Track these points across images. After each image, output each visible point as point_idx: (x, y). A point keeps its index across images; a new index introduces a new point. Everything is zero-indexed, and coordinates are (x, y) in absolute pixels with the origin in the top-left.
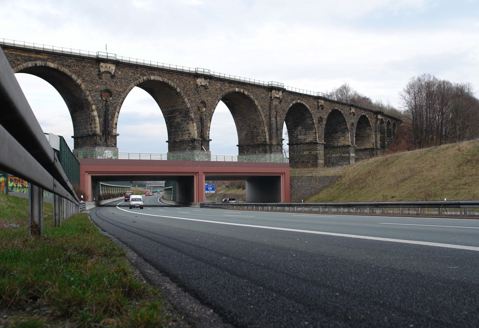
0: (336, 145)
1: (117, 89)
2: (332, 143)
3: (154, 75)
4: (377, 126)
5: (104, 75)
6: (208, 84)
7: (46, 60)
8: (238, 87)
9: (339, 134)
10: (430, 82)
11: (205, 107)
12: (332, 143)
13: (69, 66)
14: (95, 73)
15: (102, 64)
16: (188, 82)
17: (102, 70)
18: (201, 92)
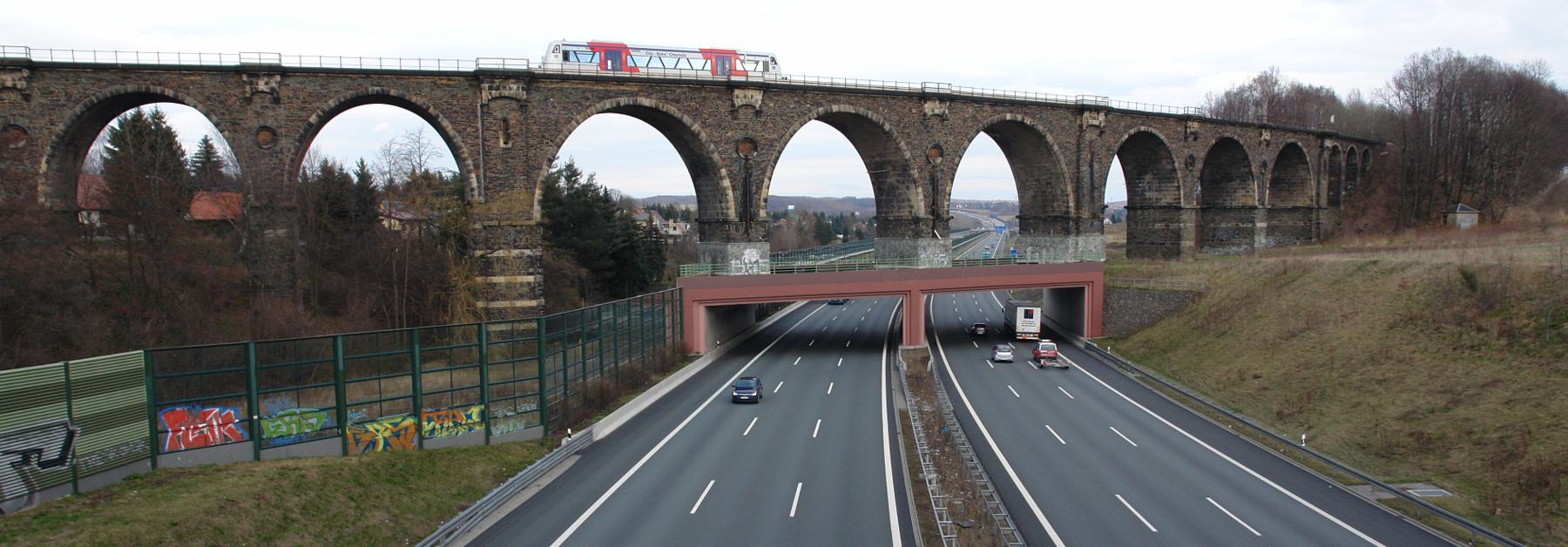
1: (767, 136)
2: (1220, 201)
3: (839, 102)
4: (1322, 163)
8: (1011, 112)
9: (1235, 184)
12: (1220, 201)
13: (678, 101)
14: (724, 108)
15: (737, 92)
17: (738, 102)
18: (932, 127)
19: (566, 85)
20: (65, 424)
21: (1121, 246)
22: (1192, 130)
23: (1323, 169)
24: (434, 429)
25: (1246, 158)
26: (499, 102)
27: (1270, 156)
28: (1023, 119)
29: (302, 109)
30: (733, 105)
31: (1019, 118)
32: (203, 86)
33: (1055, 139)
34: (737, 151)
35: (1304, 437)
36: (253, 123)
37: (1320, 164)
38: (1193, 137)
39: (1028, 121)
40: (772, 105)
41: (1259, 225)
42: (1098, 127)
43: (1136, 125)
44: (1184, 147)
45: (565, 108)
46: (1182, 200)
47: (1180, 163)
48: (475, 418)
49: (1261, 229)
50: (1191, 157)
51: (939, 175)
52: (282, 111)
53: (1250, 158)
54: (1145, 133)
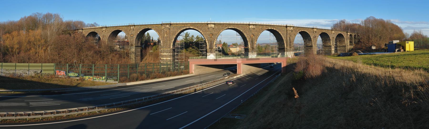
0: (327, 45)
1: (215, 33)
2: (326, 45)
3: (231, 26)
4: (348, 37)
5: (210, 29)
6: (255, 27)
7: (190, 26)
8: (270, 27)
9: (328, 41)
10: (355, 28)
11: (254, 36)
12: (326, 45)
13: (198, 27)
14: (207, 28)
15: (209, 25)
16: (246, 27)
17: (209, 27)
18: (252, 31)
19: (177, 25)
20: (41, 70)
21: (410, 49)
22: (315, 31)
23: (348, 38)
24: (96, 79)
25: (329, 36)
26: (166, 29)
27: (335, 36)
28: (273, 29)
29: (137, 31)
30: (208, 27)
31: (272, 29)
32: (125, 29)
33: (281, 32)
34: (209, 36)
35: (242, 101)
36: (130, 33)
37: (347, 38)
38: (315, 32)
39: (274, 29)
40: (216, 27)
41: (332, 49)
42: (291, 30)
43: (301, 30)
44: (313, 34)
45: (177, 29)
46: (313, 44)
47: (312, 37)
48: (104, 78)
49: (333, 50)
50: (315, 36)
51: (253, 40)
52: (134, 32)
53: (330, 36)
54: (303, 31)
